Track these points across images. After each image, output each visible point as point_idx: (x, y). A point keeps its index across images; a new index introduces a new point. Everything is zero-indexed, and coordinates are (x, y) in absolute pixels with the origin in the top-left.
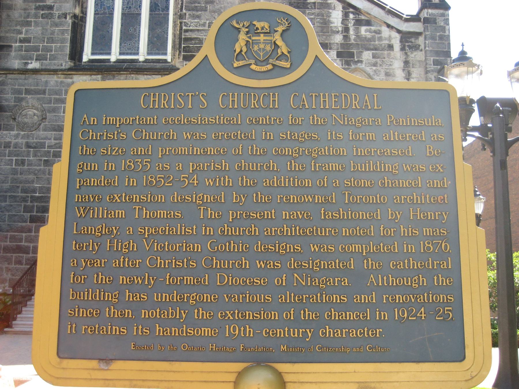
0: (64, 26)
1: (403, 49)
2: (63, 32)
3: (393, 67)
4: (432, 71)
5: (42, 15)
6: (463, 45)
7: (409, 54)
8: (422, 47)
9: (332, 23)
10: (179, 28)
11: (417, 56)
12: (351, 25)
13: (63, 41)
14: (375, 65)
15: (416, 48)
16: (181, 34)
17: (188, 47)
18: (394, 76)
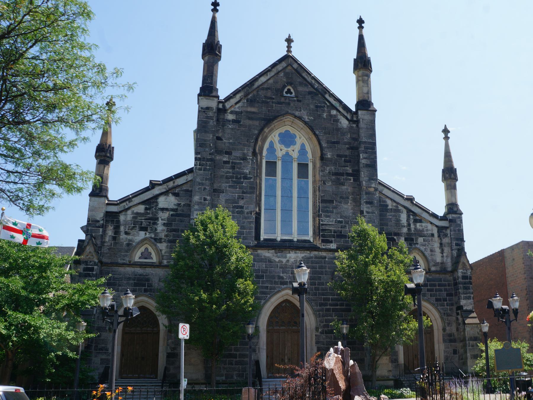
0: (250, 219)
1: (439, 236)
2: (250, 223)
3: (434, 247)
4: (455, 249)
5: (237, 211)
6: (289, 41)
7: (442, 239)
8: (449, 235)
9: (401, 221)
10: (318, 223)
11: (446, 240)
12: (411, 221)
13: (250, 228)
14: (425, 245)
15: (446, 235)
16: (319, 226)
17: (324, 234)
18: (435, 252)
